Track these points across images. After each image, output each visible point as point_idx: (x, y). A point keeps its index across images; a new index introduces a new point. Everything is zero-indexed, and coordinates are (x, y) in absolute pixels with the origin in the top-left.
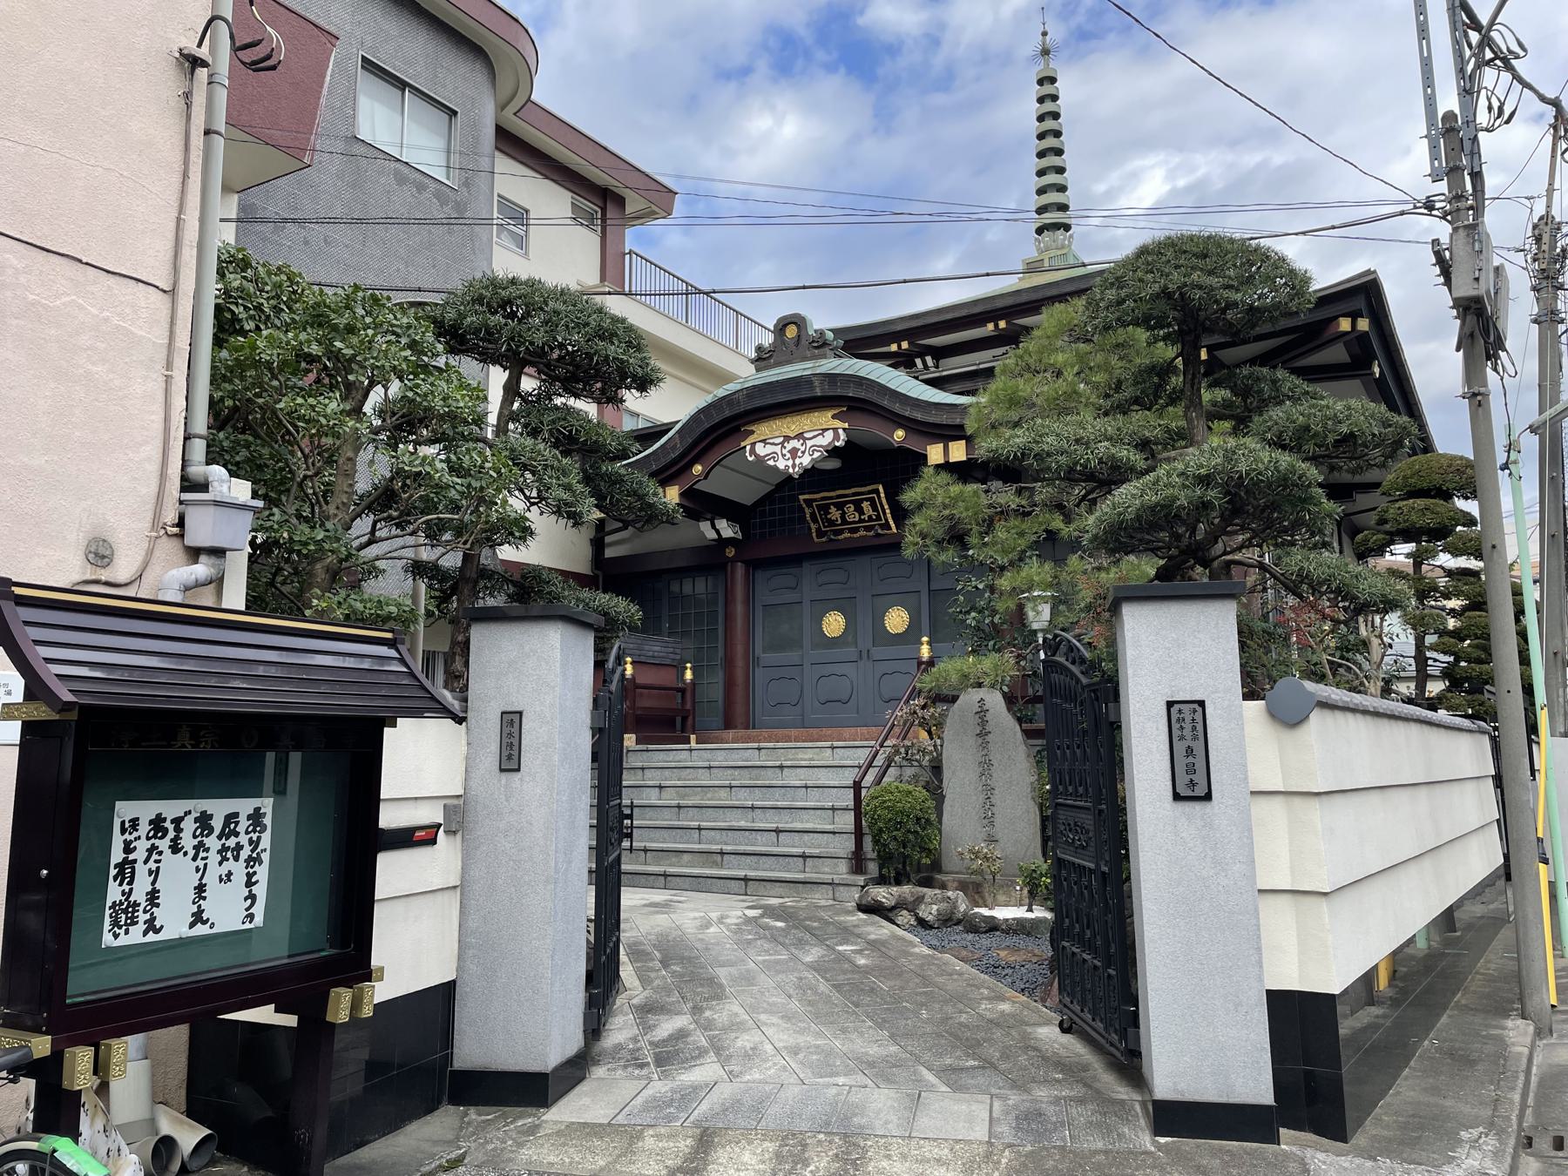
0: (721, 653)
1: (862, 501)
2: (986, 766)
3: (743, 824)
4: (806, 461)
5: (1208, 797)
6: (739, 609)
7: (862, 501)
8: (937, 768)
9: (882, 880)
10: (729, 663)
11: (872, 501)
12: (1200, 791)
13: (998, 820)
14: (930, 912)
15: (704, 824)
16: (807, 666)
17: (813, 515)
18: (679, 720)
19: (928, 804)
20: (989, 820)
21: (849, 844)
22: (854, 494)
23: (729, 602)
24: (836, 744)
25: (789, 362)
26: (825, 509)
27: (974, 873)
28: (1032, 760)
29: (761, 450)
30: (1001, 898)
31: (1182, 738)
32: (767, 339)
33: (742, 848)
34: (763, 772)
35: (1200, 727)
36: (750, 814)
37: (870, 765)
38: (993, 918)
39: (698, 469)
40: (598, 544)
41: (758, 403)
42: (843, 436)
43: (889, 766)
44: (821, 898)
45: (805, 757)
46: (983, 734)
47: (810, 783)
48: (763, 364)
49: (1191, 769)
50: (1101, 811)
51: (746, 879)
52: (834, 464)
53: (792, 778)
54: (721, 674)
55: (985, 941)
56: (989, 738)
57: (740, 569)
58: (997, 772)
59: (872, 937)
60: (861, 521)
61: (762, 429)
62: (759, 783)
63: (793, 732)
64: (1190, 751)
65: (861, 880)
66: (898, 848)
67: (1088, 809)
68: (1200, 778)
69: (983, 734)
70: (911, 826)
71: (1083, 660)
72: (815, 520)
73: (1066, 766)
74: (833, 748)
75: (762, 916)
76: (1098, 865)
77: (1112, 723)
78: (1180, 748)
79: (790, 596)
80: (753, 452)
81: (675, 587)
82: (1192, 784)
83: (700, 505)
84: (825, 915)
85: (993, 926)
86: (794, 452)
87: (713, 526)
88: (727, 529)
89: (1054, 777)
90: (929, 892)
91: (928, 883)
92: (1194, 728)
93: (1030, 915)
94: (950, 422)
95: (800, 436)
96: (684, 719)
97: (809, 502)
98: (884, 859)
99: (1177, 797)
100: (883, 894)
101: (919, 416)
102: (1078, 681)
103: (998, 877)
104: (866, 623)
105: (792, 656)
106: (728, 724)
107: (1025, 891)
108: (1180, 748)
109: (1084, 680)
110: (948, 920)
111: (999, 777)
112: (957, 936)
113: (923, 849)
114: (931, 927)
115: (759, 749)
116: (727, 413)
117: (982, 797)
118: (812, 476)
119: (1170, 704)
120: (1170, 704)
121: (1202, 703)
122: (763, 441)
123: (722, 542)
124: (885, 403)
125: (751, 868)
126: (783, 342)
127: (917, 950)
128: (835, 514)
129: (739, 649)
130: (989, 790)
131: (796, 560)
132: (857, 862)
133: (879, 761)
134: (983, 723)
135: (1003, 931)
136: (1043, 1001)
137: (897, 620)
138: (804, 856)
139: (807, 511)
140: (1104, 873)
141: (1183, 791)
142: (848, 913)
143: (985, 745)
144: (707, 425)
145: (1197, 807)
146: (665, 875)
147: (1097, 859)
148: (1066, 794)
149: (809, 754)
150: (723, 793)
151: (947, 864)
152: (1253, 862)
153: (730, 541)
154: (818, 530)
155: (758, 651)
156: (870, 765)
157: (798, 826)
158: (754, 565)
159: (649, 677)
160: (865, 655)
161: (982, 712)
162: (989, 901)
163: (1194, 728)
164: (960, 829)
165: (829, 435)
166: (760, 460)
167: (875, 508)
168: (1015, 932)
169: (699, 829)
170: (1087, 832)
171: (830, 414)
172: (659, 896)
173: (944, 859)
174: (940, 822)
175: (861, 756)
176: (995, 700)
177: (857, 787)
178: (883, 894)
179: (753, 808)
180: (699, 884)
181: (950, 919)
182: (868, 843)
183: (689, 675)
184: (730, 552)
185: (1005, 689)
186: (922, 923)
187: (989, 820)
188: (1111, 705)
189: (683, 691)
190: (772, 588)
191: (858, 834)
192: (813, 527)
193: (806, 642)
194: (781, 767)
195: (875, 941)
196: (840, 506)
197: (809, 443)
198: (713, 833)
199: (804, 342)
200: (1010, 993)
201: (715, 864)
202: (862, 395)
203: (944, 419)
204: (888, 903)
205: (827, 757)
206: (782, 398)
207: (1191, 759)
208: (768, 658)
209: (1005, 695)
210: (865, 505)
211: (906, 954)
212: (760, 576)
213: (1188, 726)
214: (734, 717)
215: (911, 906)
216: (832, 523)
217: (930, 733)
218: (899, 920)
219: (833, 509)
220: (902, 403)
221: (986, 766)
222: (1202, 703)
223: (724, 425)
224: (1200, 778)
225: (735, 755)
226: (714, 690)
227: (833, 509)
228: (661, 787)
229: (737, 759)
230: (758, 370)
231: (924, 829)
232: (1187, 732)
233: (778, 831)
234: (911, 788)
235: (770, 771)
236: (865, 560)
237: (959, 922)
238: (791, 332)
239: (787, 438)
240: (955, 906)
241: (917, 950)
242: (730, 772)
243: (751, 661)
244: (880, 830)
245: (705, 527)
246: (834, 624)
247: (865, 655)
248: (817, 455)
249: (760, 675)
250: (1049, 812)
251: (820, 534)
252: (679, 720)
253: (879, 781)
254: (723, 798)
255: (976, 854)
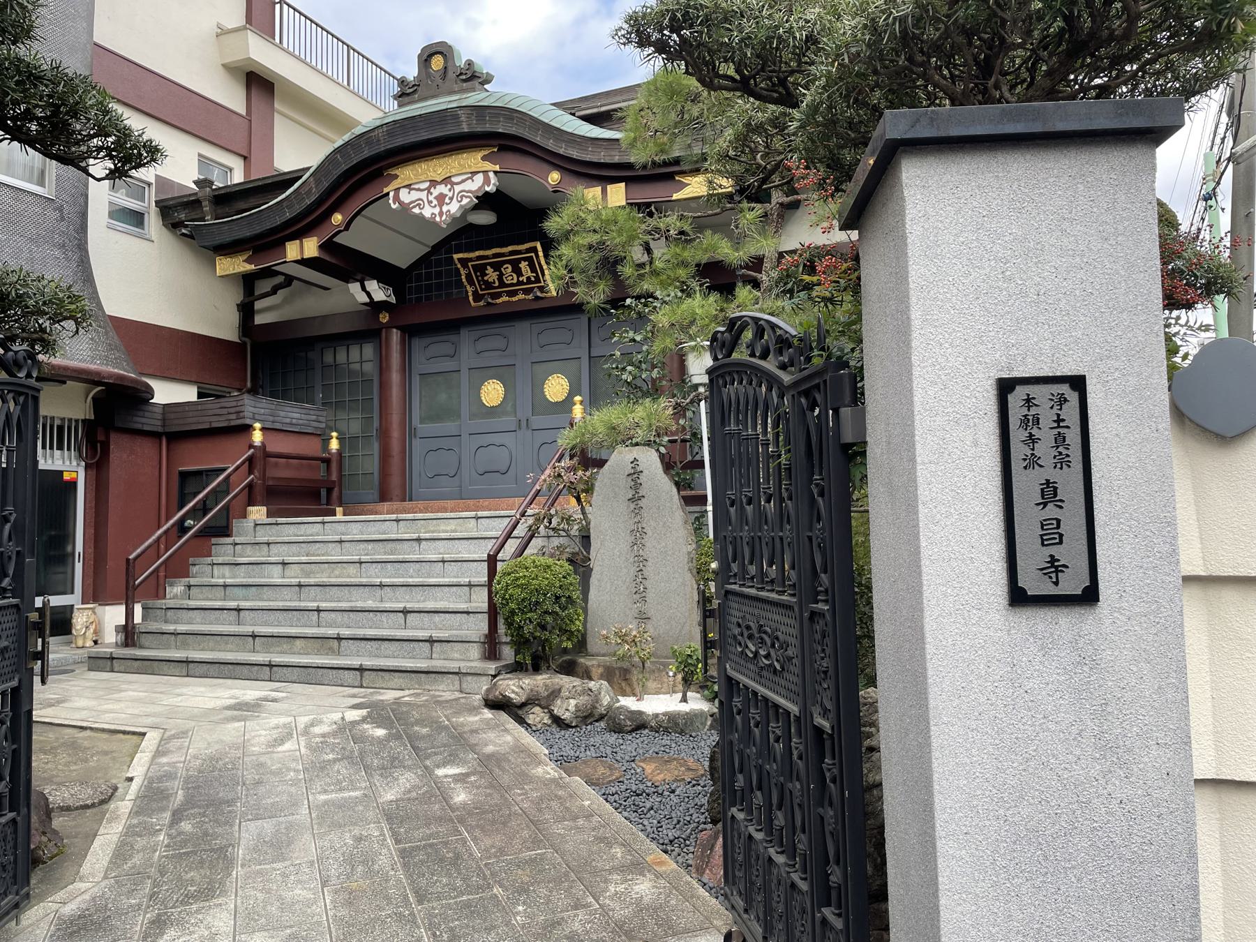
0: (376, 424)
1: (519, 260)
2: (638, 534)
3: (370, 604)
4: (454, 208)
5: (1090, 596)
6: (395, 377)
7: (519, 260)
8: (586, 539)
9: (517, 668)
10: (384, 434)
11: (530, 260)
12: (1072, 583)
13: (650, 595)
14: (566, 708)
15: (323, 605)
16: (465, 437)
17: (469, 276)
18: (323, 493)
19: (570, 579)
20: (640, 594)
21: (482, 625)
22: (512, 253)
23: (383, 368)
24: (480, 514)
25: (433, 97)
26: (481, 269)
27: (622, 658)
28: (690, 527)
29: (405, 196)
30: (651, 685)
31: (1032, 462)
32: (411, 71)
33: (361, 632)
34: (398, 546)
35: (1073, 436)
36: (378, 592)
37: (509, 536)
38: (640, 713)
39: (337, 218)
40: (246, 310)
41: (400, 141)
42: (493, 179)
43: (532, 537)
44: (446, 690)
45: (447, 528)
46: (635, 499)
47: (447, 557)
48: (406, 99)
49: (1052, 534)
50: (814, 615)
51: (361, 669)
52: (486, 218)
53: (431, 552)
54: (376, 446)
55: (631, 745)
56: (642, 503)
57: (395, 335)
58: (649, 541)
59: (490, 749)
60: (520, 283)
61: (406, 173)
62: (392, 557)
63: (450, 504)
64: (1049, 493)
65: (492, 667)
66: (535, 631)
67: (788, 607)
68: (1072, 552)
69: (635, 499)
70: (548, 606)
71: (783, 343)
72: (471, 283)
73: (745, 533)
74: (477, 518)
75: (364, 720)
76: (804, 709)
77: (846, 447)
78: (1027, 485)
79: (448, 365)
80: (396, 198)
81: (328, 358)
82: (1054, 567)
83: (344, 263)
84: (441, 715)
85: (640, 724)
86: (441, 199)
87: (363, 288)
88: (379, 292)
89: (724, 549)
90: (566, 682)
91: (569, 669)
92: (1060, 440)
93: (684, 708)
94: (608, 160)
95: (447, 180)
96: (330, 491)
97: (464, 262)
98: (520, 643)
99: (1018, 597)
100: (514, 687)
101: (574, 154)
102: (772, 381)
103: (648, 664)
104: (525, 393)
105: (449, 427)
106: (384, 497)
107: (680, 677)
108: (1027, 485)
109: (786, 378)
110: (588, 717)
111: (652, 547)
112: (600, 737)
113: (563, 631)
114: (568, 726)
115: (397, 521)
116: (366, 153)
117: (633, 570)
118: (464, 235)
119: (1005, 387)
120: (1005, 387)
121: (1078, 383)
122: (408, 186)
123: (375, 307)
124: (538, 139)
125: (371, 655)
126: (429, 75)
127: (539, 771)
128: (492, 275)
129: (395, 418)
130: (641, 561)
131: (452, 326)
132: (491, 649)
133: (521, 530)
134: (637, 486)
135: (652, 729)
136: (700, 871)
137: (556, 387)
138: (431, 641)
139: (463, 272)
140: (819, 731)
141: (1032, 583)
142: (473, 710)
143: (638, 511)
144: (344, 167)
145: (1063, 621)
146: (271, 666)
147: (805, 697)
148: (743, 575)
149: (452, 525)
150: (352, 569)
151: (594, 644)
152: (1188, 743)
153: (383, 305)
154: (475, 293)
155: (416, 421)
156: (509, 536)
157: (430, 605)
158: (411, 332)
159: (281, 445)
160: (524, 424)
161: (635, 474)
162: (638, 691)
163: (1060, 440)
164: (608, 607)
165: (479, 179)
166: (405, 208)
167: (533, 270)
168: (666, 730)
169: (318, 610)
170: (785, 646)
171: (480, 155)
172: (250, 691)
173: (589, 639)
174: (586, 599)
175: (497, 528)
176: (650, 460)
177: (492, 560)
178: (514, 687)
179: (381, 586)
180: (309, 675)
181: (591, 715)
182: (502, 628)
183: (334, 445)
184: (384, 318)
185: (663, 450)
186: (557, 721)
187: (640, 594)
188: (846, 412)
189: (327, 461)
190: (430, 355)
191: (493, 612)
192: (470, 289)
193: (465, 411)
194: (419, 540)
195: (490, 756)
196: (497, 267)
197: (457, 188)
198: (333, 615)
199: (451, 75)
200: (654, 853)
201: (331, 652)
202: (512, 130)
203: (601, 156)
204: (517, 698)
205: (471, 528)
206: (425, 135)
207: (1051, 511)
208: (424, 428)
209: (662, 457)
210: (523, 265)
211: (523, 778)
212: (417, 343)
213: (1046, 435)
214: (391, 489)
215: (544, 701)
216: (489, 285)
217: (578, 499)
218: (531, 719)
219: (490, 270)
220: (556, 139)
221: (638, 534)
222: (1078, 383)
223: (364, 168)
224: (1072, 552)
225: (372, 527)
226: (369, 462)
227: (490, 270)
228: (284, 564)
229: (373, 532)
230: (400, 106)
231: (564, 608)
232: (1045, 449)
233: (405, 612)
234: (550, 561)
235: (406, 545)
236: (523, 327)
237: (601, 717)
238: (437, 63)
239: (434, 183)
240: (597, 700)
241: (539, 771)
242: (362, 546)
243: (409, 432)
244: (513, 612)
245: (355, 288)
246: (493, 392)
247: (524, 424)
248: (465, 201)
249: (418, 446)
250: (716, 603)
251: (477, 297)
252: (323, 493)
253: (521, 551)
254: (351, 575)
255: (623, 638)
